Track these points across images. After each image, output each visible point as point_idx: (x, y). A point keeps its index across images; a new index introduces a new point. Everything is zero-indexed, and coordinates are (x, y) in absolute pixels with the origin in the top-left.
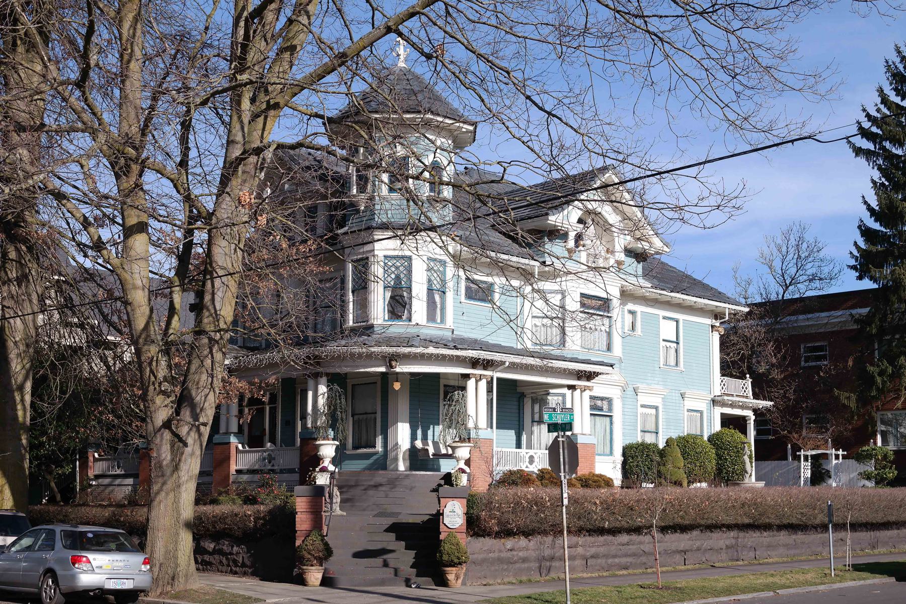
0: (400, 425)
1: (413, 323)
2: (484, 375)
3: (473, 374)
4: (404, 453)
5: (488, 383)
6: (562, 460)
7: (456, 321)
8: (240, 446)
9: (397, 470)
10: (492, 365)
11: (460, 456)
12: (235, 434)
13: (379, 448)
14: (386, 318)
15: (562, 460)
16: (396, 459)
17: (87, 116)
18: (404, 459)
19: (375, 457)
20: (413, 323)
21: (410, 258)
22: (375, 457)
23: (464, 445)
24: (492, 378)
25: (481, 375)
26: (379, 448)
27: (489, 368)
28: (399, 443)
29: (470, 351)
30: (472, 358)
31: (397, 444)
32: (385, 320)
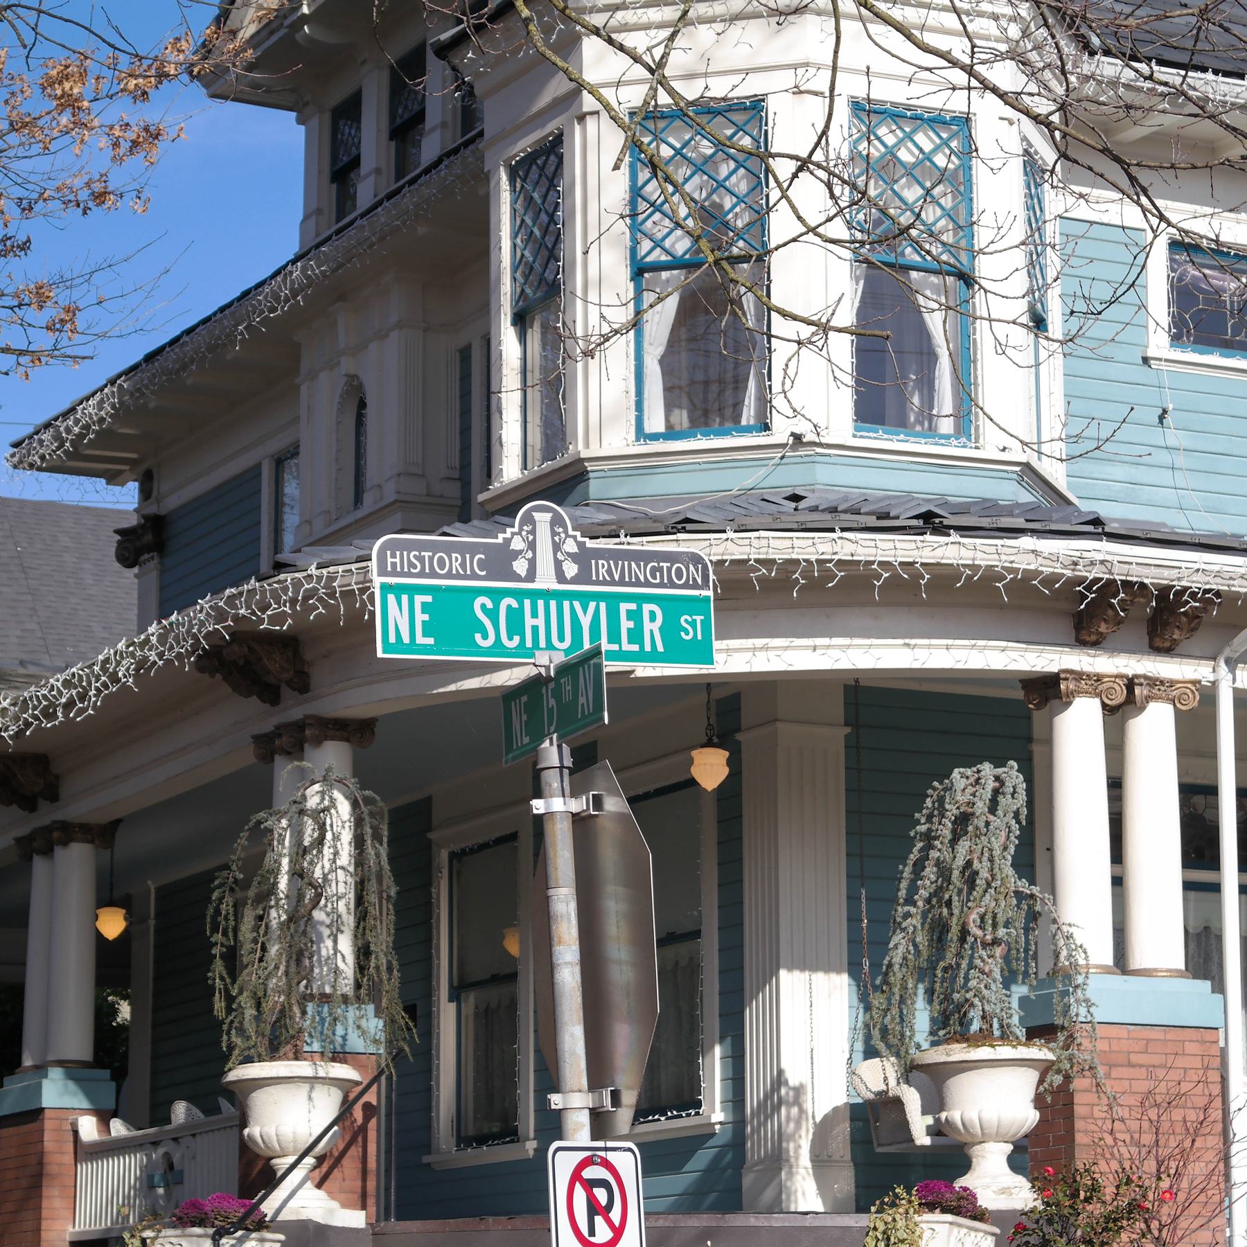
0: (791, 983)
1: (781, 430)
2: (1153, 682)
3: (1078, 676)
4: (824, 1129)
5: (1182, 719)
6: (568, 976)
7: (1078, 406)
8: (89, 1128)
9: (777, 1206)
10: (1195, 619)
11: (972, 1116)
12: (73, 1069)
13: (717, 1113)
14: (655, 422)
15: (568, 976)
16: (777, 1161)
17: (1161, 89)
18: (820, 1161)
19: (702, 1158)
20: (781, 430)
21: (965, 120)
22: (702, 1158)
23: (983, 1053)
24: (1208, 696)
25: (1131, 683)
26: (717, 1113)
27: (1199, 641)
28: (793, 1078)
29: (1027, 542)
30: (1030, 575)
31: (779, 1080)
32: (641, 434)
